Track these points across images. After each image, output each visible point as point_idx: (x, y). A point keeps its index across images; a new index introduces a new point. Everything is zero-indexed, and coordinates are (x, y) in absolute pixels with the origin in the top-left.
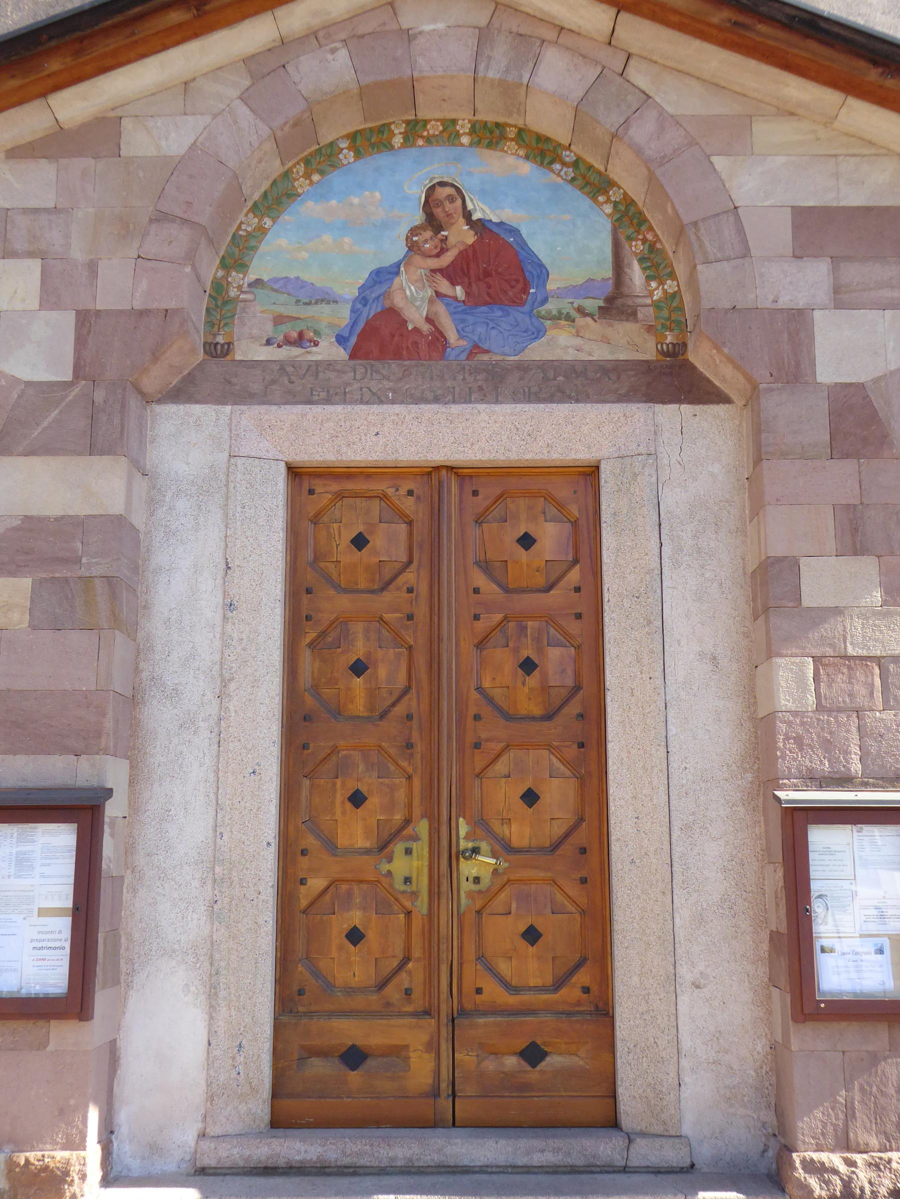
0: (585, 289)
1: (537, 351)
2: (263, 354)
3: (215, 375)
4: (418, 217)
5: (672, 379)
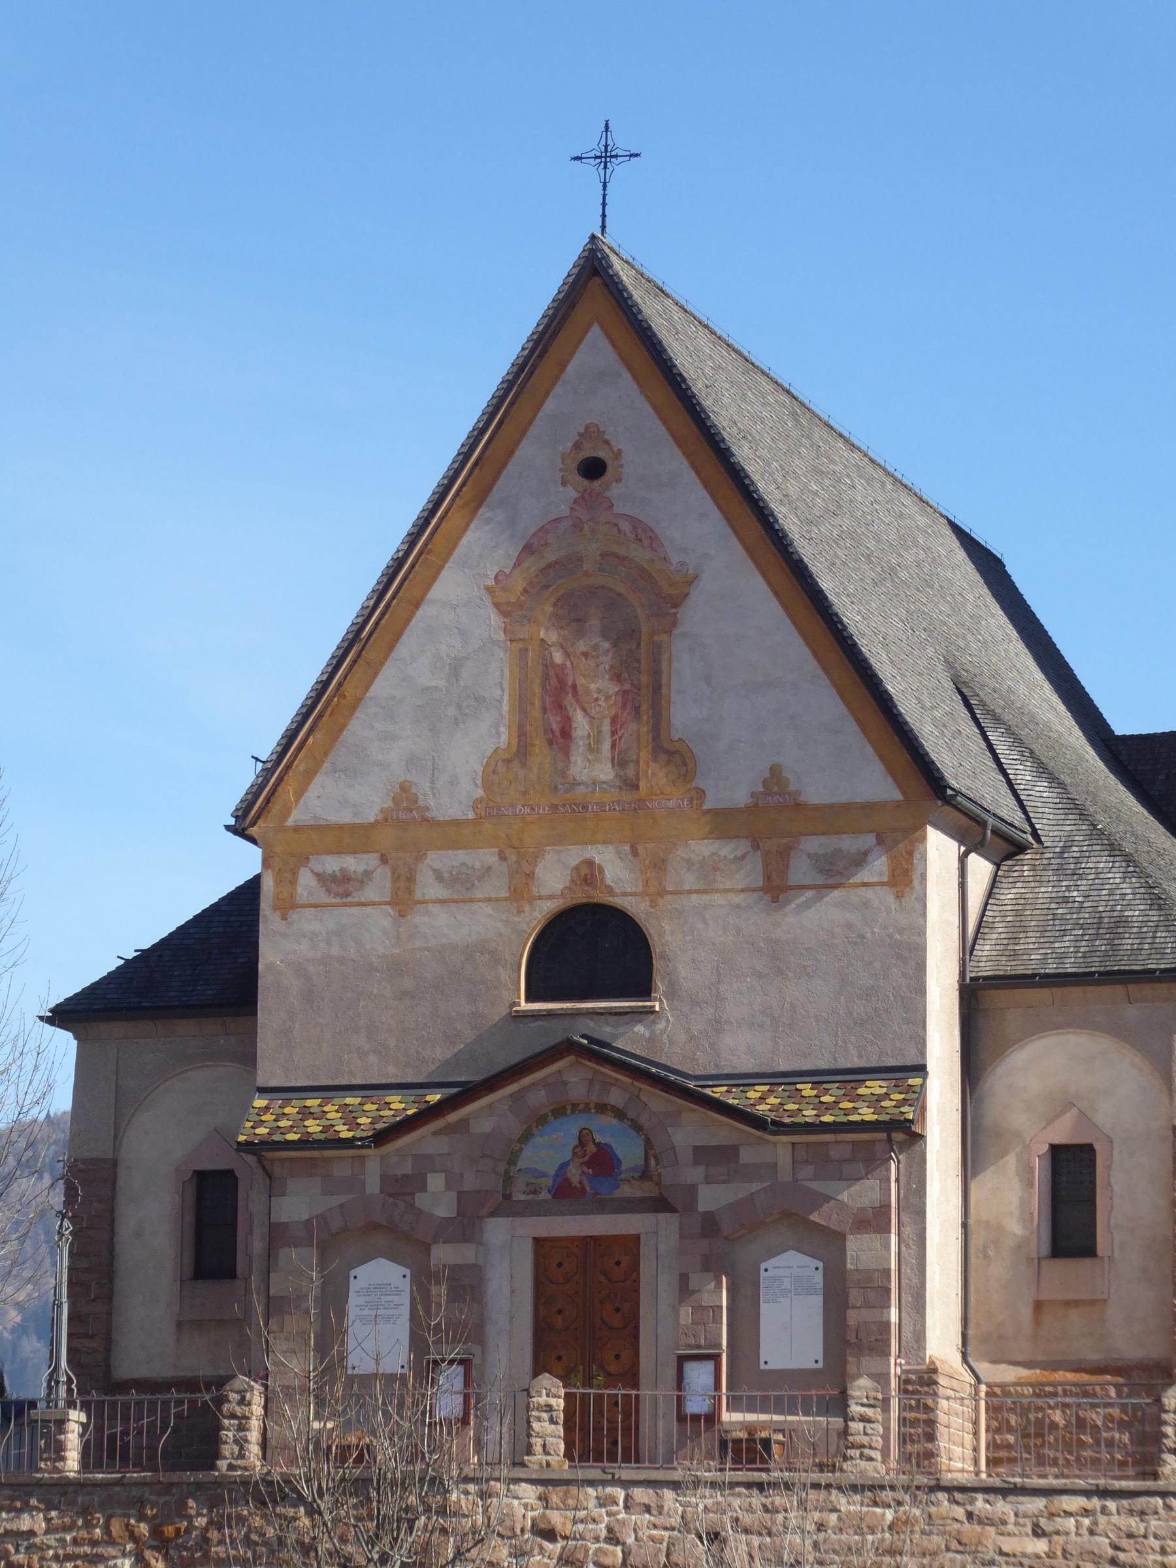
0: (633, 1170)
1: (617, 1194)
2: (523, 1197)
3: (506, 1207)
4: (576, 1142)
5: (660, 1204)
